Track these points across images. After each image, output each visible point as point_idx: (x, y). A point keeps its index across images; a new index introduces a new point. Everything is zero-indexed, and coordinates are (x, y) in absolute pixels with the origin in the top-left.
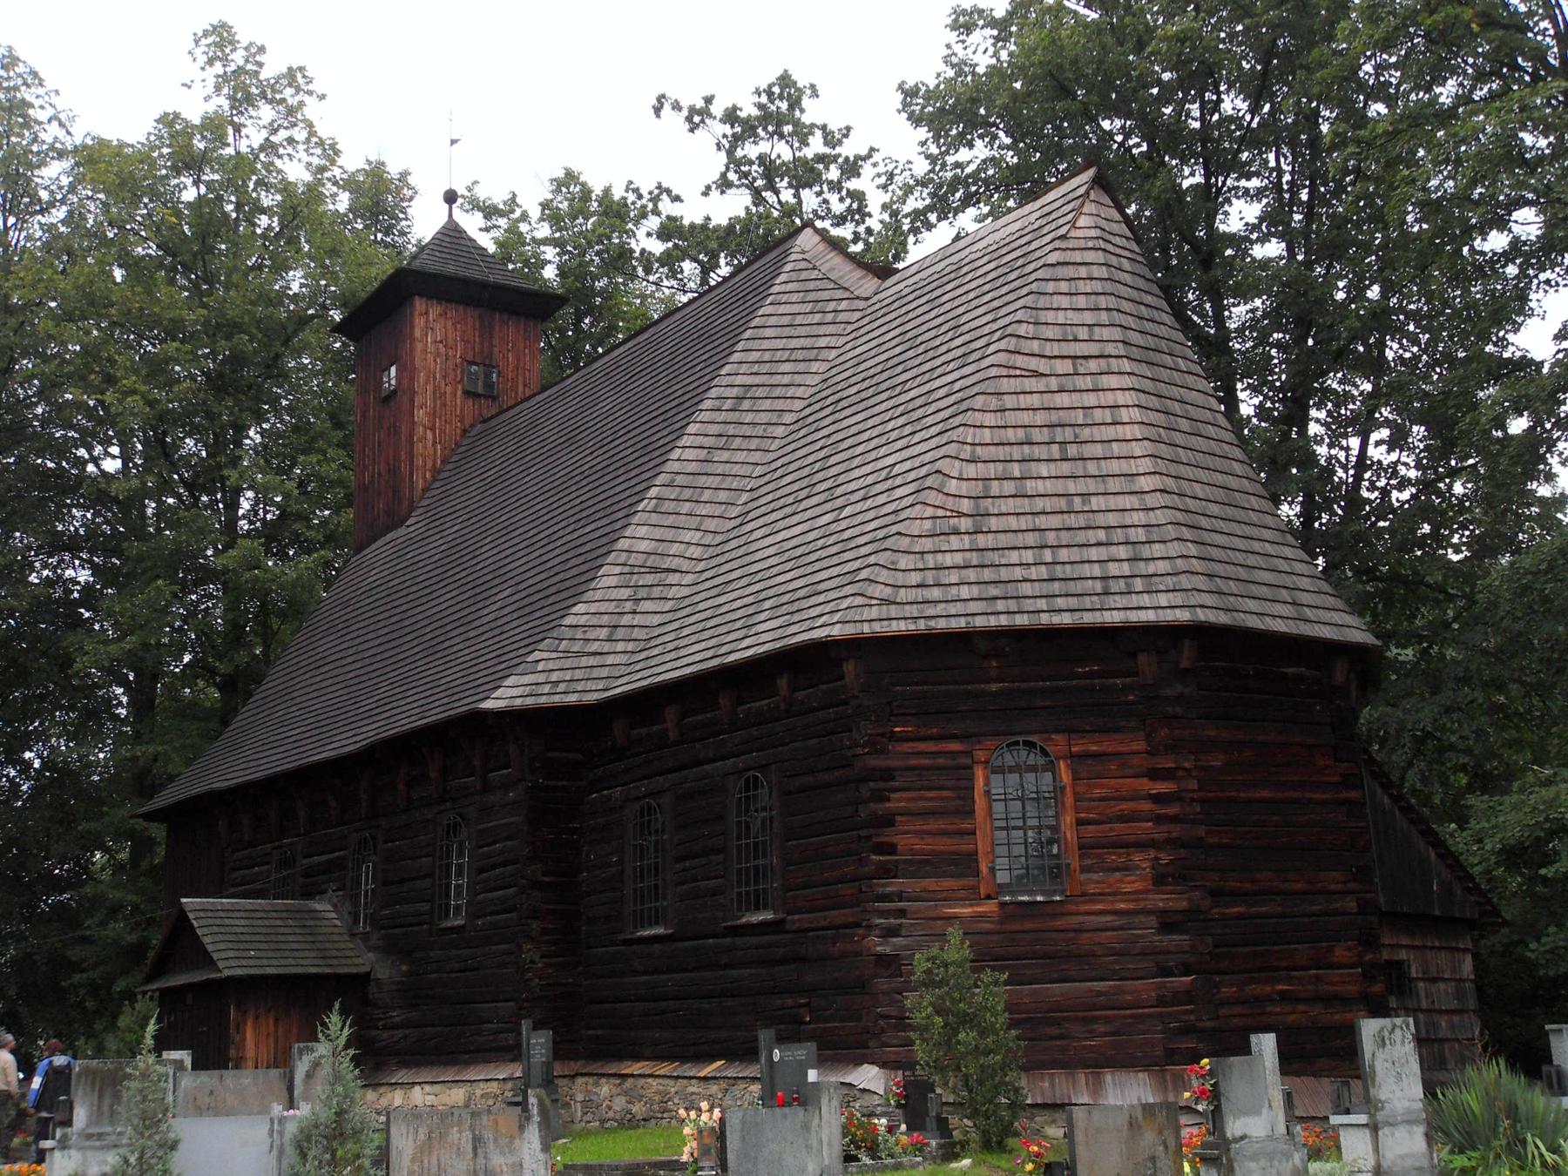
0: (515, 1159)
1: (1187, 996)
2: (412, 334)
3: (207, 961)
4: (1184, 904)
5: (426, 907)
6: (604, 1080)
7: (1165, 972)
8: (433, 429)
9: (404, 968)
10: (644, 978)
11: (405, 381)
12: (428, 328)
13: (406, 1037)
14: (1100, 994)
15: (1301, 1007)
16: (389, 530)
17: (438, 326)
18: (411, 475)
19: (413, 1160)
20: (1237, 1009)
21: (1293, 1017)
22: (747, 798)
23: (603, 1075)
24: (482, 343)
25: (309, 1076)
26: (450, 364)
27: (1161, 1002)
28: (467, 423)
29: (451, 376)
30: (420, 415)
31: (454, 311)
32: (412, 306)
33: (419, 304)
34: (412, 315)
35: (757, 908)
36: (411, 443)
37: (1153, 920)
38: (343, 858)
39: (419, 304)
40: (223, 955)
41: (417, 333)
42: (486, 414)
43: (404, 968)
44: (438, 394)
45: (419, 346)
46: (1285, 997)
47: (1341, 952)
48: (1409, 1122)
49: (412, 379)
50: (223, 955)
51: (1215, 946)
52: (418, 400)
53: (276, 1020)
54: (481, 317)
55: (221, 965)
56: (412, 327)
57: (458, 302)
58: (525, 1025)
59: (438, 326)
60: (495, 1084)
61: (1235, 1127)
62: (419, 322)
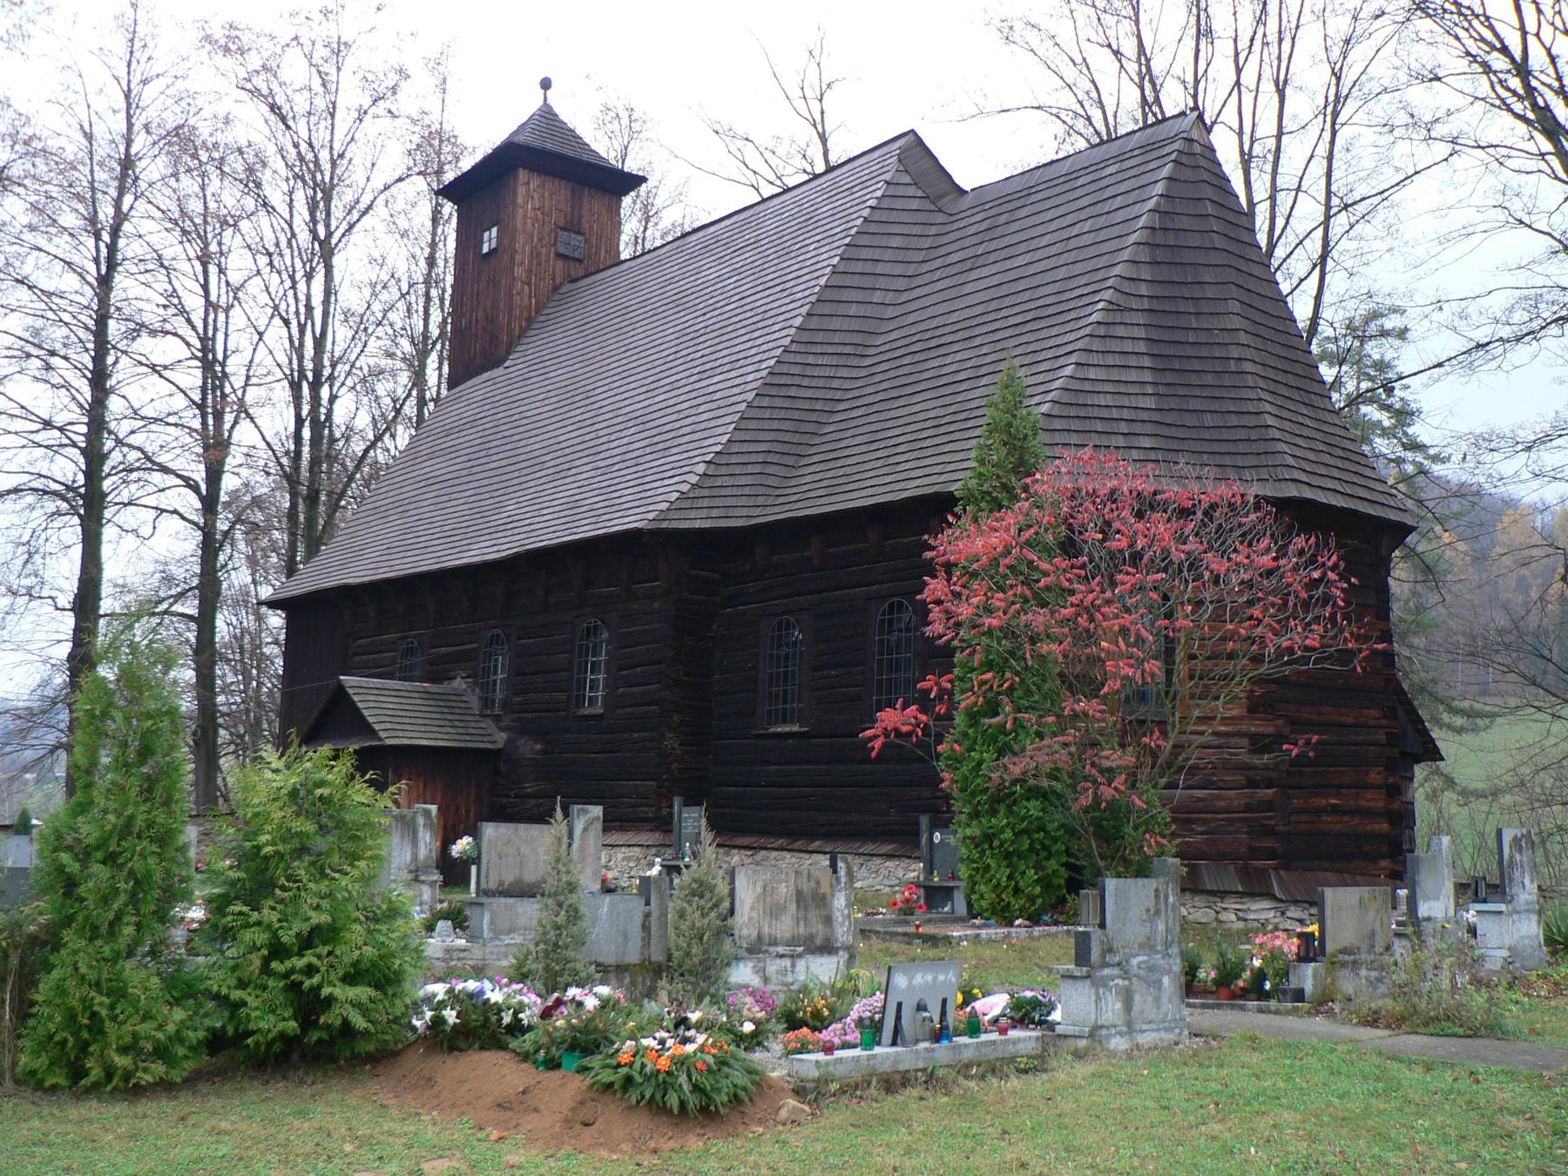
0: (824, 913)
1: (1268, 805)
2: (514, 202)
3: (373, 733)
4: (1271, 730)
5: (563, 696)
6: (735, 851)
7: (1252, 784)
8: (529, 284)
9: (538, 747)
10: (773, 768)
11: (506, 242)
12: (529, 196)
13: (538, 806)
14: (1199, 799)
15: (1345, 819)
16: (484, 369)
17: (536, 195)
18: (509, 323)
19: (752, 909)
20: (1303, 818)
21: (1339, 826)
22: (891, 620)
23: (734, 847)
24: (580, 216)
25: (585, 830)
26: (546, 229)
27: (1248, 808)
28: (558, 280)
29: (546, 240)
30: (519, 271)
31: (552, 184)
32: (516, 177)
33: (522, 175)
34: (515, 183)
35: (784, 722)
36: (511, 296)
37: (1245, 742)
38: (473, 650)
39: (522, 175)
40: (383, 726)
41: (520, 200)
42: (574, 276)
43: (538, 747)
44: (535, 254)
45: (521, 211)
46: (1335, 810)
47: (1375, 776)
48: (1528, 911)
49: (513, 240)
50: (383, 726)
51: (1291, 765)
52: (518, 258)
53: (425, 785)
54: (573, 190)
55: (382, 734)
56: (515, 195)
57: (554, 175)
58: (677, 802)
59: (536, 195)
60: (638, 849)
61: (1424, 910)
62: (521, 190)
